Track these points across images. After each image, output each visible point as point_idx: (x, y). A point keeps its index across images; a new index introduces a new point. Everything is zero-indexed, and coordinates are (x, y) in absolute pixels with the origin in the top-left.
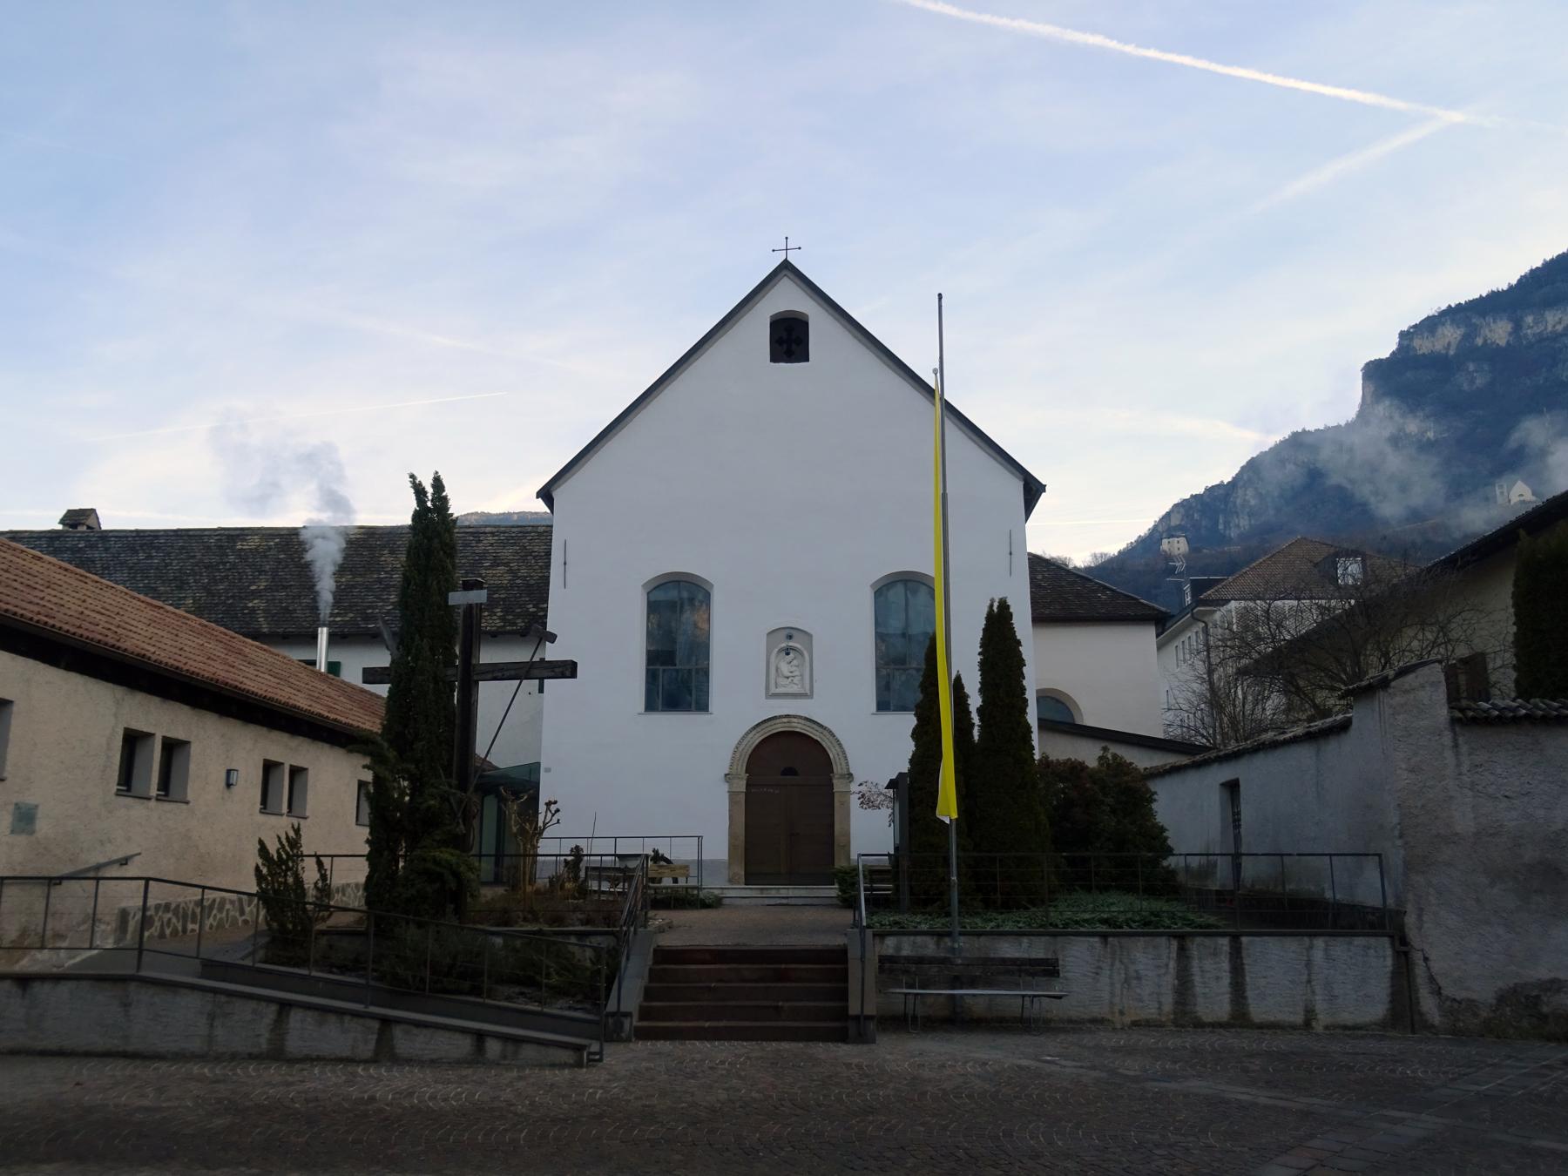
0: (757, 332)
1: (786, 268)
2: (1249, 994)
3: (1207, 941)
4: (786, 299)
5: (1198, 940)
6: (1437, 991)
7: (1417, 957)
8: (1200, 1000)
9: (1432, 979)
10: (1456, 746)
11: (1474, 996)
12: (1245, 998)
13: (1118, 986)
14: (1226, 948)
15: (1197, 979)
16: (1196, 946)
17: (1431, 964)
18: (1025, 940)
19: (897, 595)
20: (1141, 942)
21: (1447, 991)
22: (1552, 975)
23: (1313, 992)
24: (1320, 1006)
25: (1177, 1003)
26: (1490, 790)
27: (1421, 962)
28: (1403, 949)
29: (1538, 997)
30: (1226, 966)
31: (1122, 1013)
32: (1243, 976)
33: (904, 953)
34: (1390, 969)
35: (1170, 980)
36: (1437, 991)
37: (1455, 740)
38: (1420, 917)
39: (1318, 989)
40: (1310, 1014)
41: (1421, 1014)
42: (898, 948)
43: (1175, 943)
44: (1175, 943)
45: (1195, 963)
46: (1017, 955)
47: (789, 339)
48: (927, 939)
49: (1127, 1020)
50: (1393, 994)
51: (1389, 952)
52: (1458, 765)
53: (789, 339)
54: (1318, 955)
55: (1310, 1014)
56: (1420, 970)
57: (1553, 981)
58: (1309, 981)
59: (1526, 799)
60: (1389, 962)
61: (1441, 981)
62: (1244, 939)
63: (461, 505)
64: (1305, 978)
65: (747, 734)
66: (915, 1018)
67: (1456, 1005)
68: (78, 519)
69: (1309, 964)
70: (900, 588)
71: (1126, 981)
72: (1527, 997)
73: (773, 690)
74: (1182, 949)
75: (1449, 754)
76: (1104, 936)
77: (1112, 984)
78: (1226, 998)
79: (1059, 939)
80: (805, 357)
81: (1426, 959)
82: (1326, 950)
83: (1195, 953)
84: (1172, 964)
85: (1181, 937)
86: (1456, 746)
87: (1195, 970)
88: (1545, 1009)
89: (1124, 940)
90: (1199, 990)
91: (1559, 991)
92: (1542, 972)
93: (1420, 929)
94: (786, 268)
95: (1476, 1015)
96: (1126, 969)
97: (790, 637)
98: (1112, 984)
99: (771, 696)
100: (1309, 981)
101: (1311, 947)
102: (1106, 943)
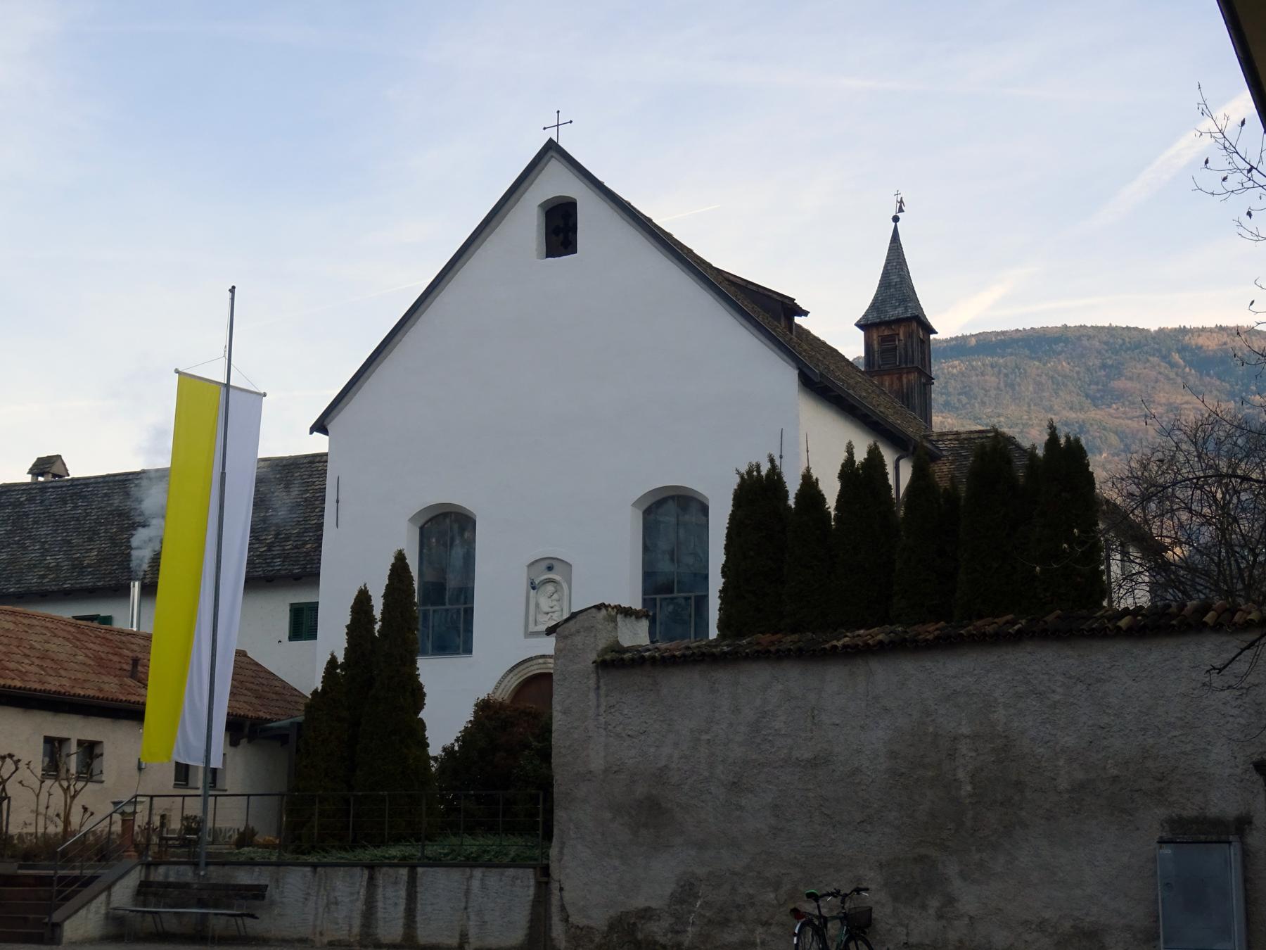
0: (527, 224)
1: (552, 149)
2: (418, 919)
3: (391, 871)
4: (555, 184)
5: (385, 869)
6: (566, 919)
7: (554, 886)
8: (381, 923)
9: (563, 908)
10: (598, 688)
11: (592, 924)
12: (415, 922)
13: (321, 910)
14: (405, 878)
15: (380, 904)
16: (382, 876)
17: (565, 894)
18: (257, 869)
19: (669, 516)
20: (341, 872)
21: (575, 919)
22: (647, 904)
23: (468, 918)
24: (472, 932)
25: (363, 925)
26: (619, 729)
27: (556, 892)
28: (545, 879)
29: (634, 924)
30: (403, 893)
31: (321, 934)
32: (415, 903)
33: (171, 879)
34: (531, 898)
35: (360, 905)
36: (566, 919)
37: (598, 681)
38: (562, 849)
39: (473, 917)
40: (464, 937)
41: (552, 940)
42: (167, 875)
43: (404, 872)
44: (366, 872)
45: (380, 890)
46: (249, 882)
47: (560, 229)
48: (187, 867)
49: (325, 940)
50: (531, 921)
51: (532, 882)
52: (598, 706)
53: (560, 229)
54: (476, 884)
55: (464, 937)
56: (555, 900)
57: (648, 909)
58: (466, 908)
59: (643, 737)
60: (532, 891)
61: (570, 910)
62: (420, 870)
63: (951, 314)
64: (463, 905)
65: (504, 677)
66: (213, 938)
67: (578, 932)
68: (45, 466)
69: (467, 892)
70: (671, 506)
71: (328, 905)
72: (628, 924)
73: (532, 628)
74: (371, 878)
75: (592, 695)
76: (314, 866)
77: (316, 909)
78: (401, 922)
79: (282, 868)
80: (575, 251)
81: (561, 889)
82: (482, 880)
83: (380, 882)
84: (363, 891)
85: (371, 867)
86: (598, 688)
87: (380, 897)
88: (640, 936)
89: (329, 870)
90: (380, 914)
91: (650, 919)
92: (640, 902)
93: (560, 861)
94: (552, 149)
95: (592, 941)
96: (328, 896)
97: (550, 568)
98: (316, 909)
99: (530, 634)
100: (466, 908)
101: (471, 876)
102: (315, 872)
